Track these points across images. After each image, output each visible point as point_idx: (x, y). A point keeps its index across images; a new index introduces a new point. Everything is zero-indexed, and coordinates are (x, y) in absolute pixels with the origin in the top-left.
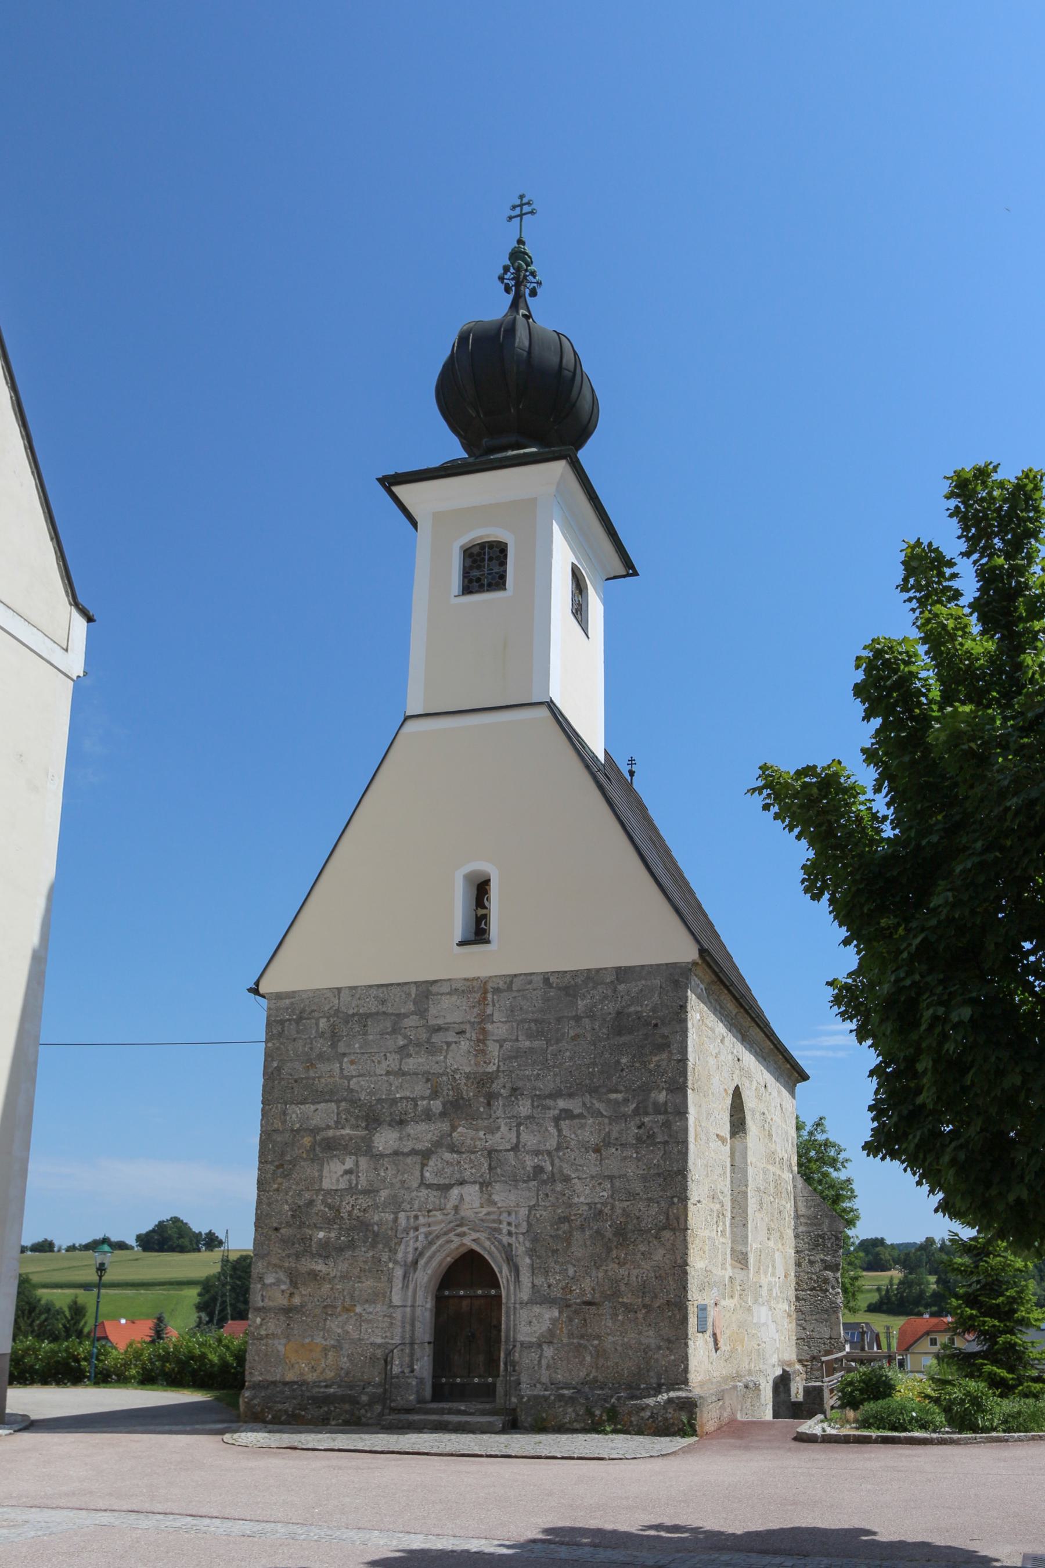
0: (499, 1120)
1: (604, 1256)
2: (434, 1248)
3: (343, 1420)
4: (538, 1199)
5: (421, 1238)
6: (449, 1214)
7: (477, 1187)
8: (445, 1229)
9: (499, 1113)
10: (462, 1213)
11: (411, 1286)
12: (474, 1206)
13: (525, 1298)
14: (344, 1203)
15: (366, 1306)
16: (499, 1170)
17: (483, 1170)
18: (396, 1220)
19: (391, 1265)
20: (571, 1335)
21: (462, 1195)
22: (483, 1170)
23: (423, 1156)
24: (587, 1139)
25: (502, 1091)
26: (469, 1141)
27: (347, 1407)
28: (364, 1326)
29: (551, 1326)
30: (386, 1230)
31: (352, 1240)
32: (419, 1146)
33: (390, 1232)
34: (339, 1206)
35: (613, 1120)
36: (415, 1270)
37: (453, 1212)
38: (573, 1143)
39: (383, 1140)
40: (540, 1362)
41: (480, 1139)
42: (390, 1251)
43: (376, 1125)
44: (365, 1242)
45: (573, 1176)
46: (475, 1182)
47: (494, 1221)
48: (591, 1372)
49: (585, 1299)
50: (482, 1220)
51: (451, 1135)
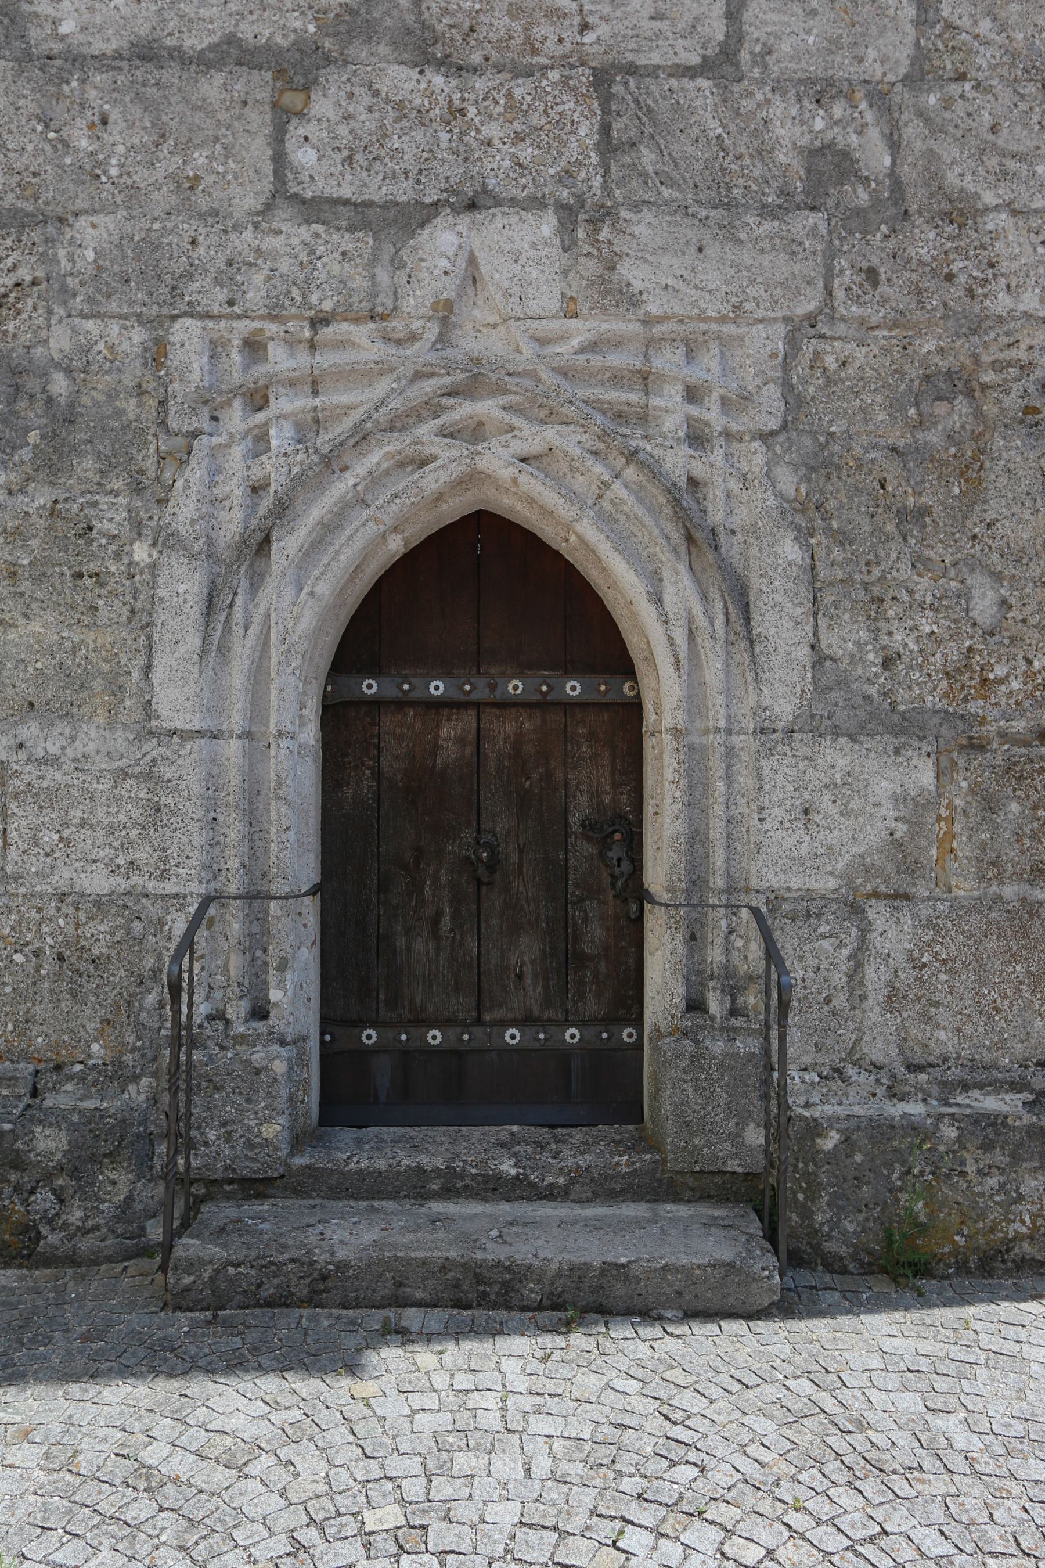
2: (342, 486)
4: (829, 292)
5: (280, 437)
6: (413, 337)
7: (548, 224)
8: (395, 403)
11: (243, 649)
12: (533, 307)
15: (29, 731)
16: (648, 158)
17: (573, 151)
19: (141, 552)
21: (472, 260)
22: (573, 151)
23: (280, 73)
29: (901, 829)
30: (111, 396)
33: (131, 407)
37: (433, 331)
42: (137, 489)
45: (989, 198)
46: (536, 203)
47: (616, 379)
50: (563, 372)
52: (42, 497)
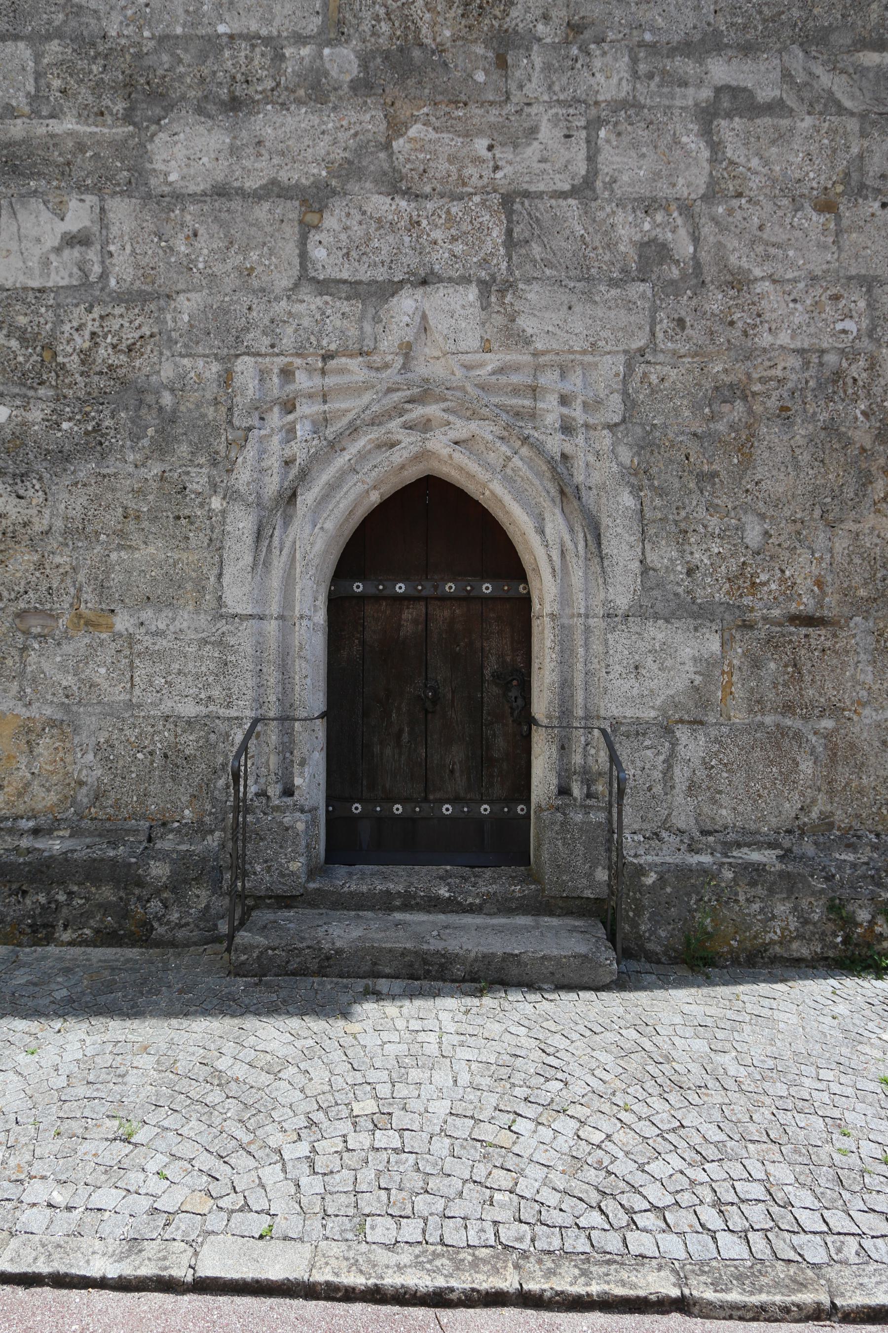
0: (534, 110)
1: (849, 493)
2: (341, 461)
3: (97, 931)
5: (303, 430)
6: (387, 366)
7: (472, 293)
8: (375, 408)
9: (534, 87)
10: (421, 369)
11: (279, 564)
12: (463, 346)
13: (623, 602)
14: (67, 328)
15: (147, 614)
16: (536, 250)
17: (488, 247)
18: (227, 378)
19: (216, 503)
20: (757, 703)
21: (424, 317)
22: (488, 247)
23: (304, 202)
24: (797, 175)
25: (540, 27)
26: (442, 166)
27: (107, 893)
28: (142, 669)
31: (97, 429)
32: (289, 175)
33: (210, 412)
34: (52, 335)
35: (874, 123)
36: (288, 520)
38: (755, 183)
39: (180, 152)
40: (668, 772)
41: (478, 160)
42: (214, 463)
43: (158, 111)
44: (136, 438)
45: (758, 272)
46: (465, 280)
47: (516, 391)
48: (814, 801)
49: (794, 608)
50: (482, 387)
51: (387, 146)
52: (156, 470)
